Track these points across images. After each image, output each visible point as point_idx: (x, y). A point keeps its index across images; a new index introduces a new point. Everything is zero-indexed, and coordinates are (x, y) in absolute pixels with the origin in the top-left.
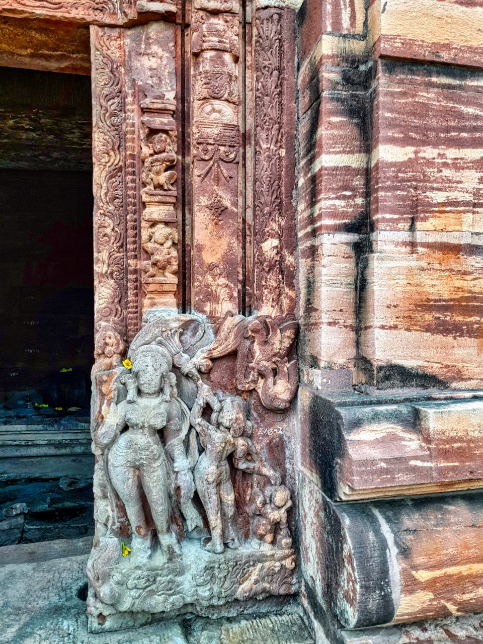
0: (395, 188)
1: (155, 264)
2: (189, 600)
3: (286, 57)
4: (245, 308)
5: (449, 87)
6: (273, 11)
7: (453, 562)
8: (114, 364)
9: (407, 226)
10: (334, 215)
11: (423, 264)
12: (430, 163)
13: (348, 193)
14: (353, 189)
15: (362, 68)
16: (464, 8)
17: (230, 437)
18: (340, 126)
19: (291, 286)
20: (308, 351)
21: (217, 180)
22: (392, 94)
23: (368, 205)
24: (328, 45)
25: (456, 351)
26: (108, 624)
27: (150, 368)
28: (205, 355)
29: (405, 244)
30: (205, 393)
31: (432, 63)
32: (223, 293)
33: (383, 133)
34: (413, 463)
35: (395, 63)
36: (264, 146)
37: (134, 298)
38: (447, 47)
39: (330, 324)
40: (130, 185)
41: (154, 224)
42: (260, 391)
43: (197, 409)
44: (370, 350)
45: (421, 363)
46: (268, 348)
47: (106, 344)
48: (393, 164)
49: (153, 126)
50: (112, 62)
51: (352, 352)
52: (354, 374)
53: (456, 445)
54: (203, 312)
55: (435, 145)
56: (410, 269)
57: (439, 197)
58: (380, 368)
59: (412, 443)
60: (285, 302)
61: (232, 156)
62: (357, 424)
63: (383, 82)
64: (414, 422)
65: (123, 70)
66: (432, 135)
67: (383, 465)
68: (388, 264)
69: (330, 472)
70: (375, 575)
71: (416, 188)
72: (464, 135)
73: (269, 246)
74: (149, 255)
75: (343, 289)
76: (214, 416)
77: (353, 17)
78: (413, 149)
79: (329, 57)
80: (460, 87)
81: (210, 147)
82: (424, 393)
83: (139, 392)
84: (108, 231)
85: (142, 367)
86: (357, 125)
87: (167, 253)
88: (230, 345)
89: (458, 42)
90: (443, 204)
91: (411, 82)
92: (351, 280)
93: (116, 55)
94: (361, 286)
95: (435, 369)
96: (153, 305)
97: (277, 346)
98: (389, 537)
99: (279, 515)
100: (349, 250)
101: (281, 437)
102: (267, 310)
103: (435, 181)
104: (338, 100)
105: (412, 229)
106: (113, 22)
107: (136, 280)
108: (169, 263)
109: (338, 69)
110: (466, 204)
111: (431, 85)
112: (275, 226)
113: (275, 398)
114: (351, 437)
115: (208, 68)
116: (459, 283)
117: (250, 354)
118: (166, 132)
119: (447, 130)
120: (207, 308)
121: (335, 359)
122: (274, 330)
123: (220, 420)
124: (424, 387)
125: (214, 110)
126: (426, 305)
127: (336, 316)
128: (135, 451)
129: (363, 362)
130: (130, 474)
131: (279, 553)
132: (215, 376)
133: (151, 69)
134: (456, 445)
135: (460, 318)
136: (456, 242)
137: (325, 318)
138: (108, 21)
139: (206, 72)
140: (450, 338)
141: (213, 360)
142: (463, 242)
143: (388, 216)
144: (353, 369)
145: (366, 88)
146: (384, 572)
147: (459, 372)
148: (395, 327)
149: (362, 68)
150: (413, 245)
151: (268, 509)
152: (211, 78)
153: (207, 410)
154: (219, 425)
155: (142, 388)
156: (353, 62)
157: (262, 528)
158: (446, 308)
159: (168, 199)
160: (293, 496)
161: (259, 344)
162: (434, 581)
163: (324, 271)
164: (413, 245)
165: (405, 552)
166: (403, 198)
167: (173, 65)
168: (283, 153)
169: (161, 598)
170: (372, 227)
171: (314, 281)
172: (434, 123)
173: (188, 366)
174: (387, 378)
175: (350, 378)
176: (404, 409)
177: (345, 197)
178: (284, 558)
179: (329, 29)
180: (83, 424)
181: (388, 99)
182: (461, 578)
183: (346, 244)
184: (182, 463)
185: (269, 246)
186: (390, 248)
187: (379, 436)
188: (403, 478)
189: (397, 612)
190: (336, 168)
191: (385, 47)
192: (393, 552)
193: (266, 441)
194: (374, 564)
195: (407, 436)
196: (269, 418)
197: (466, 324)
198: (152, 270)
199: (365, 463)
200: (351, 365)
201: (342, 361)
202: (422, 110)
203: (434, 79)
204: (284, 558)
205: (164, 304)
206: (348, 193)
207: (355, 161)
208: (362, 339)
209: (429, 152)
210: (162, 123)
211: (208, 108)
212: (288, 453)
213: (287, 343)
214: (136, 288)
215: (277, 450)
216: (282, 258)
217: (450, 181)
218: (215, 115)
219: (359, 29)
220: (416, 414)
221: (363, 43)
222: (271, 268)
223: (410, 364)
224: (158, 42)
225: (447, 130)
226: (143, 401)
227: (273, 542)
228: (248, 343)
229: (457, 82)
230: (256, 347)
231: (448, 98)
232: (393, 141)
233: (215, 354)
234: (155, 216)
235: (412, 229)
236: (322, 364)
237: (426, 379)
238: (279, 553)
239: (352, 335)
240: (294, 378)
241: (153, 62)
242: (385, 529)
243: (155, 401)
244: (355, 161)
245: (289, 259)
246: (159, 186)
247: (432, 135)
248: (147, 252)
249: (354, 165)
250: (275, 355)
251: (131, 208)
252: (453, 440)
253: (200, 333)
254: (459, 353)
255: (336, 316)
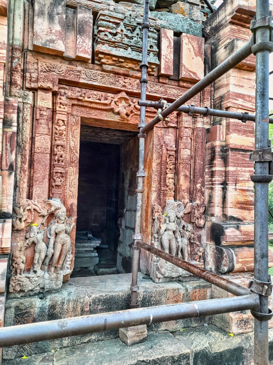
0: (232, 176)
1: (169, 189)
2: (181, 274)
3: (204, 139)
4: (191, 201)
5: (243, 154)
6: (201, 129)
7: (246, 258)
8: (161, 214)
9: (235, 185)
10: (218, 181)
11: (238, 193)
12: (239, 171)
13: (221, 176)
14: (222, 175)
15: (225, 148)
16: (246, 137)
17: (190, 234)
18: (220, 160)
19: (203, 196)
20: (210, 213)
21: (186, 168)
22: (232, 156)
23: (225, 179)
24: (217, 143)
25: (244, 213)
26: (160, 281)
27: (173, 216)
28: (183, 213)
29: (234, 189)
30: (183, 223)
31: (240, 149)
32: (186, 197)
33: (230, 164)
34: (238, 236)
35: (232, 149)
36: (198, 161)
37: (163, 197)
38: (243, 146)
39: (217, 206)
40: (163, 168)
41: (169, 178)
42: (196, 223)
43: (182, 227)
44: (227, 213)
45: (237, 216)
46: (199, 212)
47: (159, 209)
48: (232, 171)
49: (170, 154)
50: (159, 136)
51: (222, 213)
52: (222, 218)
53: (246, 233)
54: (182, 202)
55: (240, 167)
56: (235, 194)
57: (241, 179)
58: (229, 217)
59: (238, 233)
60: (202, 200)
61: (189, 163)
62: (227, 228)
63: (230, 153)
64: (238, 228)
65: (161, 138)
66: (240, 165)
67: (233, 237)
68: (231, 193)
69: (219, 240)
70: (231, 259)
71: (236, 176)
72: (246, 165)
73: (198, 186)
74: (167, 186)
75: (220, 198)
76: (186, 228)
77: (223, 137)
78: (236, 168)
79: (218, 146)
80: (246, 154)
81: (184, 160)
82: (238, 223)
83: (169, 221)
84: (156, 179)
85: (171, 215)
86: (223, 161)
87: (172, 186)
88: (189, 210)
89: (245, 145)
90: (242, 180)
91: (236, 153)
92: (222, 196)
93: (160, 134)
94: (224, 198)
95: (240, 217)
96: (169, 199)
97: (201, 211)
98: (233, 253)
99: (201, 254)
100: (221, 189)
101: (200, 235)
102: (198, 202)
103: (240, 175)
104: (220, 155)
105: (236, 185)
106: (160, 127)
107: (163, 193)
108: (173, 188)
109: (220, 148)
110: (247, 180)
111: (240, 154)
112: (200, 181)
113: (200, 224)
114: (226, 231)
115: (184, 141)
116: (245, 198)
117: (194, 213)
118: (173, 156)
119: (243, 164)
120: (182, 201)
121: (218, 215)
122: (200, 207)
123: (188, 229)
124: (238, 221)
125: (185, 151)
126: (239, 203)
127: (218, 204)
128: (170, 236)
129: (225, 215)
130: (168, 242)
131: (201, 264)
132: (184, 218)
133: (169, 139)
134: (246, 233)
135: (245, 206)
136: (244, 189)
137: (216, 205)
138: (159, 126)
139: (184, 142)
140: (243, 210)
141: (184, 214)
142: (246, 189)
143: (231, 182)
144: (222, 217)
145: (225, 153)
146: (233, 259)
147: (245, 218)
148: (232, 207)
149: (225, 148)
150: (236, 189)
151: (198, 252)
152: (185, 144)
153: (184, 227)
154: (187, 231)
155: (170, 220)
156: (223, 147)
157: (197, 257)
158: (242, 204)
159: (173, 172)
160: (204, 250)
161: (197, 210)
162: (242, 261)
163: (216, 194)
164: (236, 189)
165: (236, 255)
166: (234, 179)
167: (174, 138)
168: (202, 163)
169: (174, 274)
170: (227, 184)
171: (212, 196)
172: (240, 162)
173: (179, 216)
174: (231, 219)
175: (221, 219)
176: (235, 226)
177: (221, 177)
178: (202, 265)
179: (218, 139)
180: (78, 244)
181: (231, 157)
182: (247, 261)
183: (221, 188)
184: (179, 239)
185: (198, 186)
186: (231, 189)
187: (231, 231)
188: (237, 240)
189: (235, 268)
190: (219, 171)
191: (231, 146)
192: (234, 255)
193: (197, 235)
194: (231, 257)
195: (237, 231)
196: (198, 229)
197: (246, 207)
198: (169, 190)
199: (229, 236)
200: (221, 216)
201: (219, 215)
202: (238, 159)
203: (240, 153)
204: (202, 265)
205: (171, 199)
206: (221, 176)
207: (223, 169)
208: (224, 210)
209: (239, 169)
210: (173, 154)
211: (184, 151)
212: (202, 239)
213: (203, 210)
214: (163, 195)
215: (199, 238)
216: (201, 189)
217: (243, 175)
218: (186, 152)
219: (224, 140)
220: (238, 227)
221: (225, 143)
222: (199, 191)
223: (235, 216)
224: (171, 133)
225: (243, 164)
226: (170, 224)
227: (199, 261)
228: (194, 210)
229: (245, 153)
230: (196, 211)
231: (243, 157)
232: (232, 166)
233: (185, 213)
234: (170, 177)
235: (236, 185)
236: (215, 216)
237: (239, 220)
238: (201, 264)
239: (222, 209)
240: (205, 220)
241: (169, 137)
242: (232, 251)
243: (173, 224)
244: (223, 169)
245: (203, 189)
246: (170, 169)
247: (240, 165)
248: (167, 185)
249: (223, 170)
250: (200, 213)
251: (163, 174)
252: (246, 232)
253: (181, 207)
254: (245, 214)
255: (218, 204)
